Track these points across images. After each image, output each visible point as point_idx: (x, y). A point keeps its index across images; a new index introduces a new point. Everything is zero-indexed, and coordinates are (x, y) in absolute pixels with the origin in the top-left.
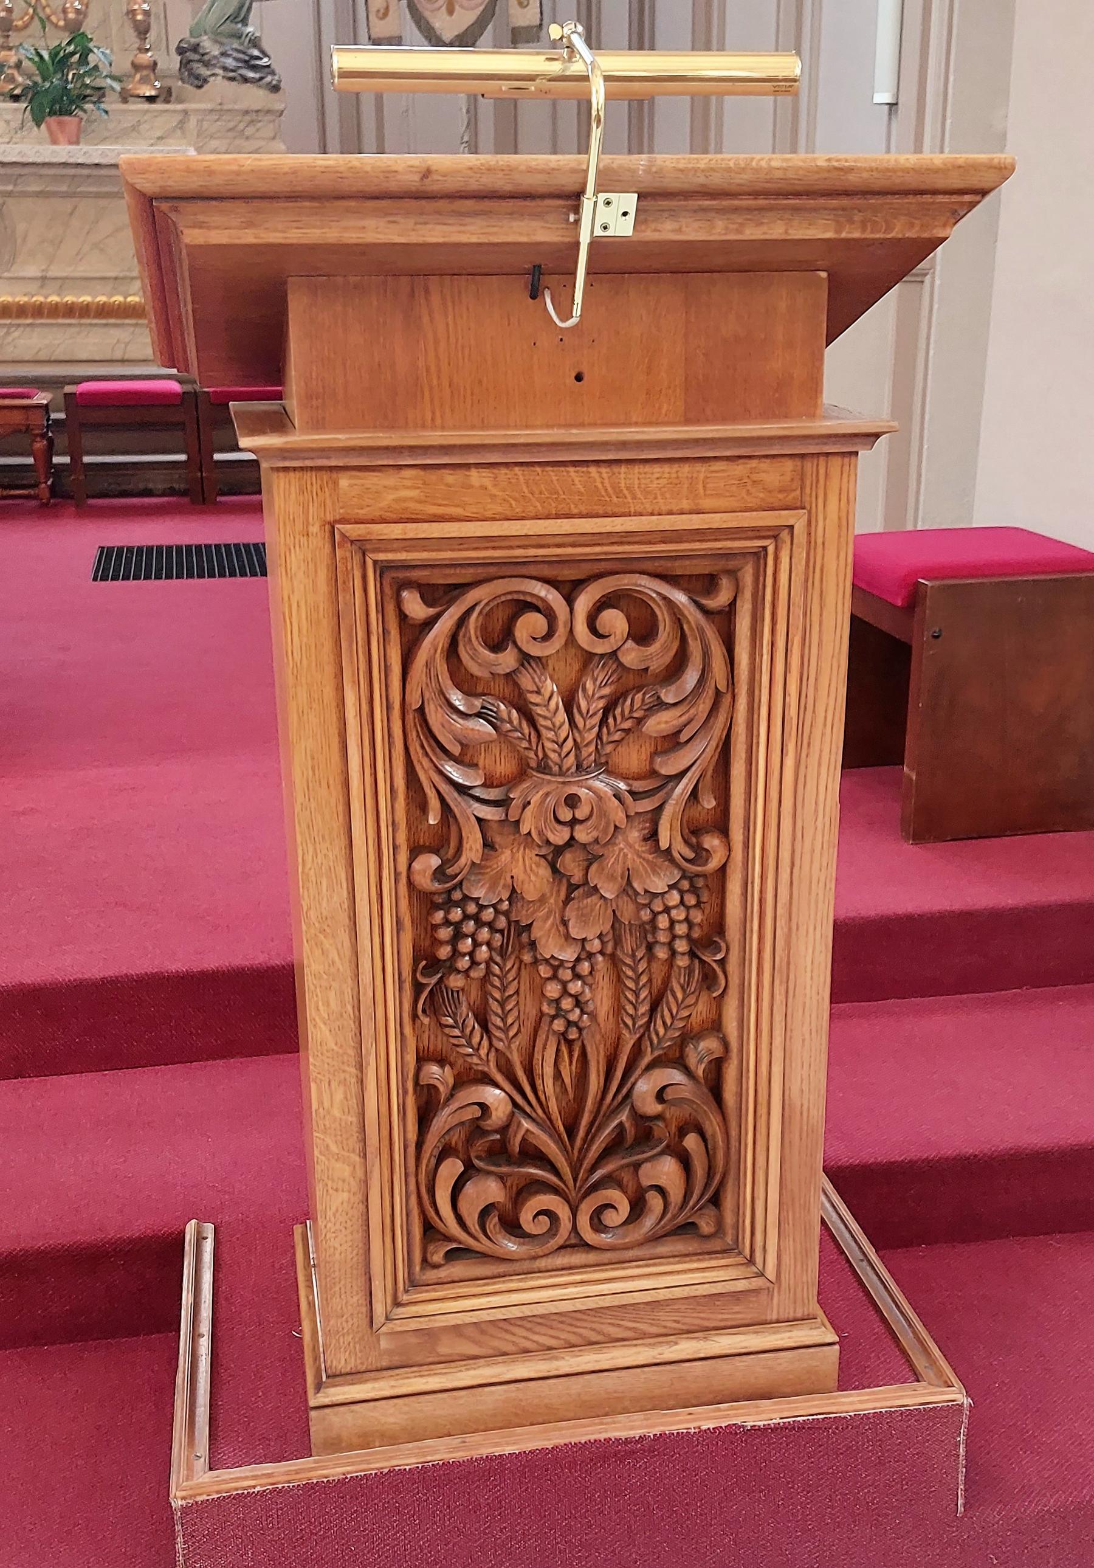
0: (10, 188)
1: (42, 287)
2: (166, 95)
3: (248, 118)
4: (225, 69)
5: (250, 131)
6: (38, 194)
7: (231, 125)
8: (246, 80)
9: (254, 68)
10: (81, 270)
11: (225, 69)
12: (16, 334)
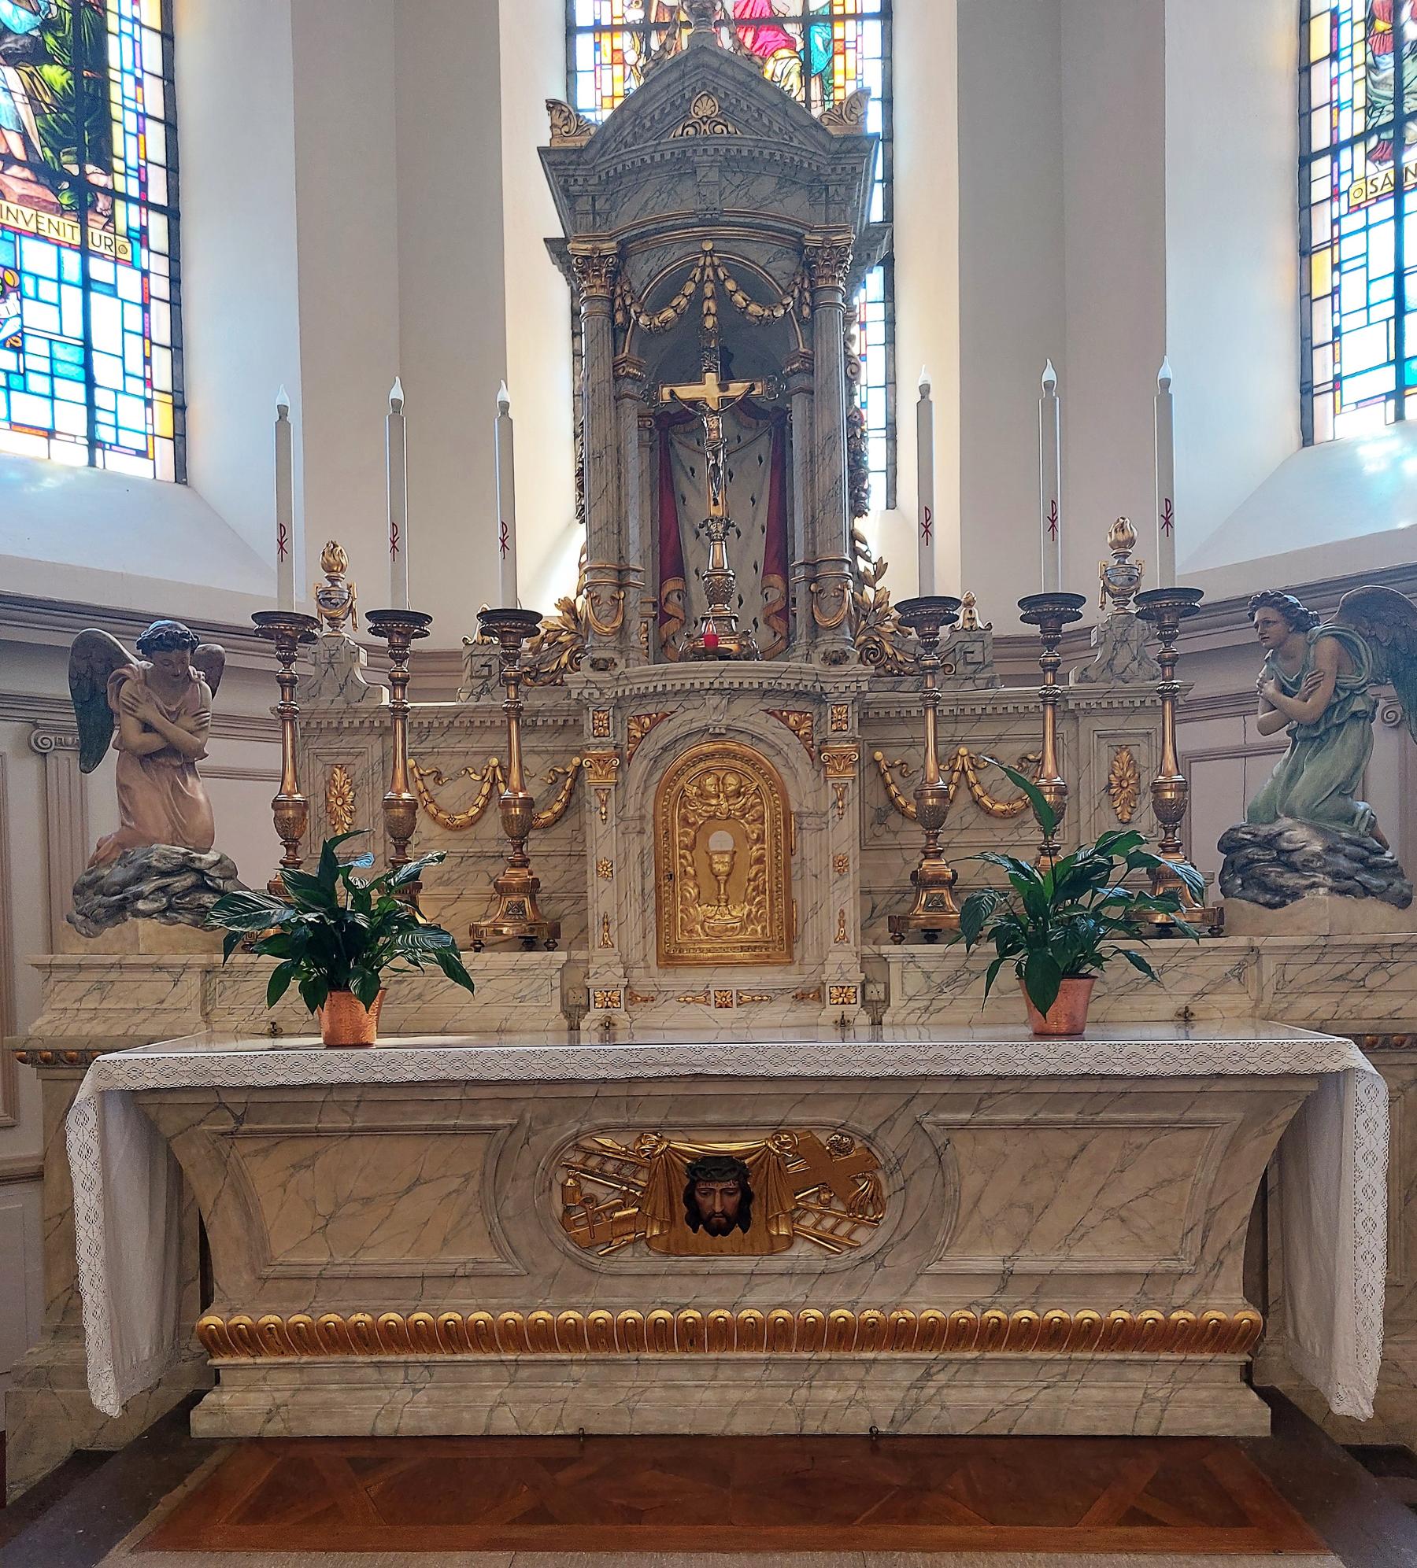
0: (965, 1116)
1: (1002, 1289)
2: (1216, 924)
3: (1374, 958)
4: (1336, 875)
5: (1374, 981)
6: (1017, 1126)
7: (1340, 970)
8: (1367, 891)
9: (1373, 869)
10: (1082, 1258)
11: (1336, 875)
12: (942, 1378)
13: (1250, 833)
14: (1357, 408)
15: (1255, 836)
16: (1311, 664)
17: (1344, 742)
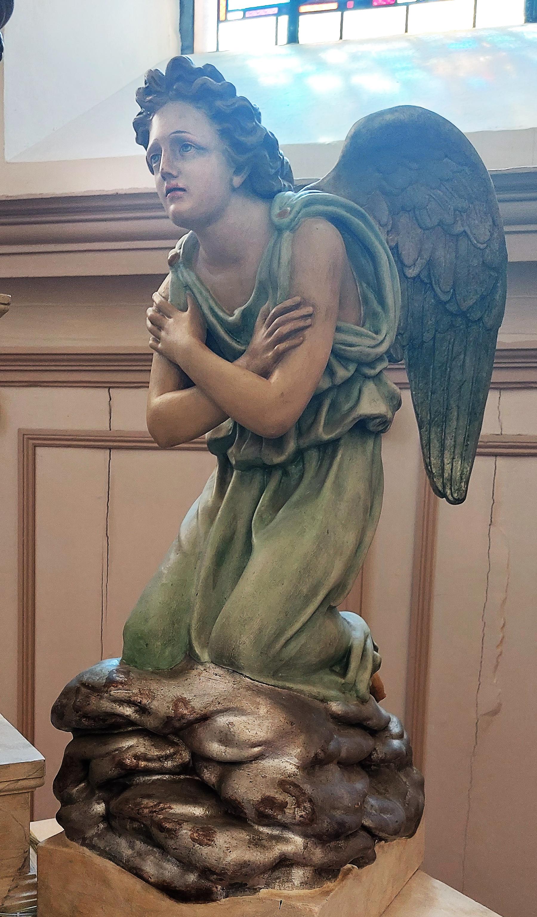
13: (129, 702)
14: (244, 17)
15: (143, 710)
16: (283, 280)
17: (338, 488)
